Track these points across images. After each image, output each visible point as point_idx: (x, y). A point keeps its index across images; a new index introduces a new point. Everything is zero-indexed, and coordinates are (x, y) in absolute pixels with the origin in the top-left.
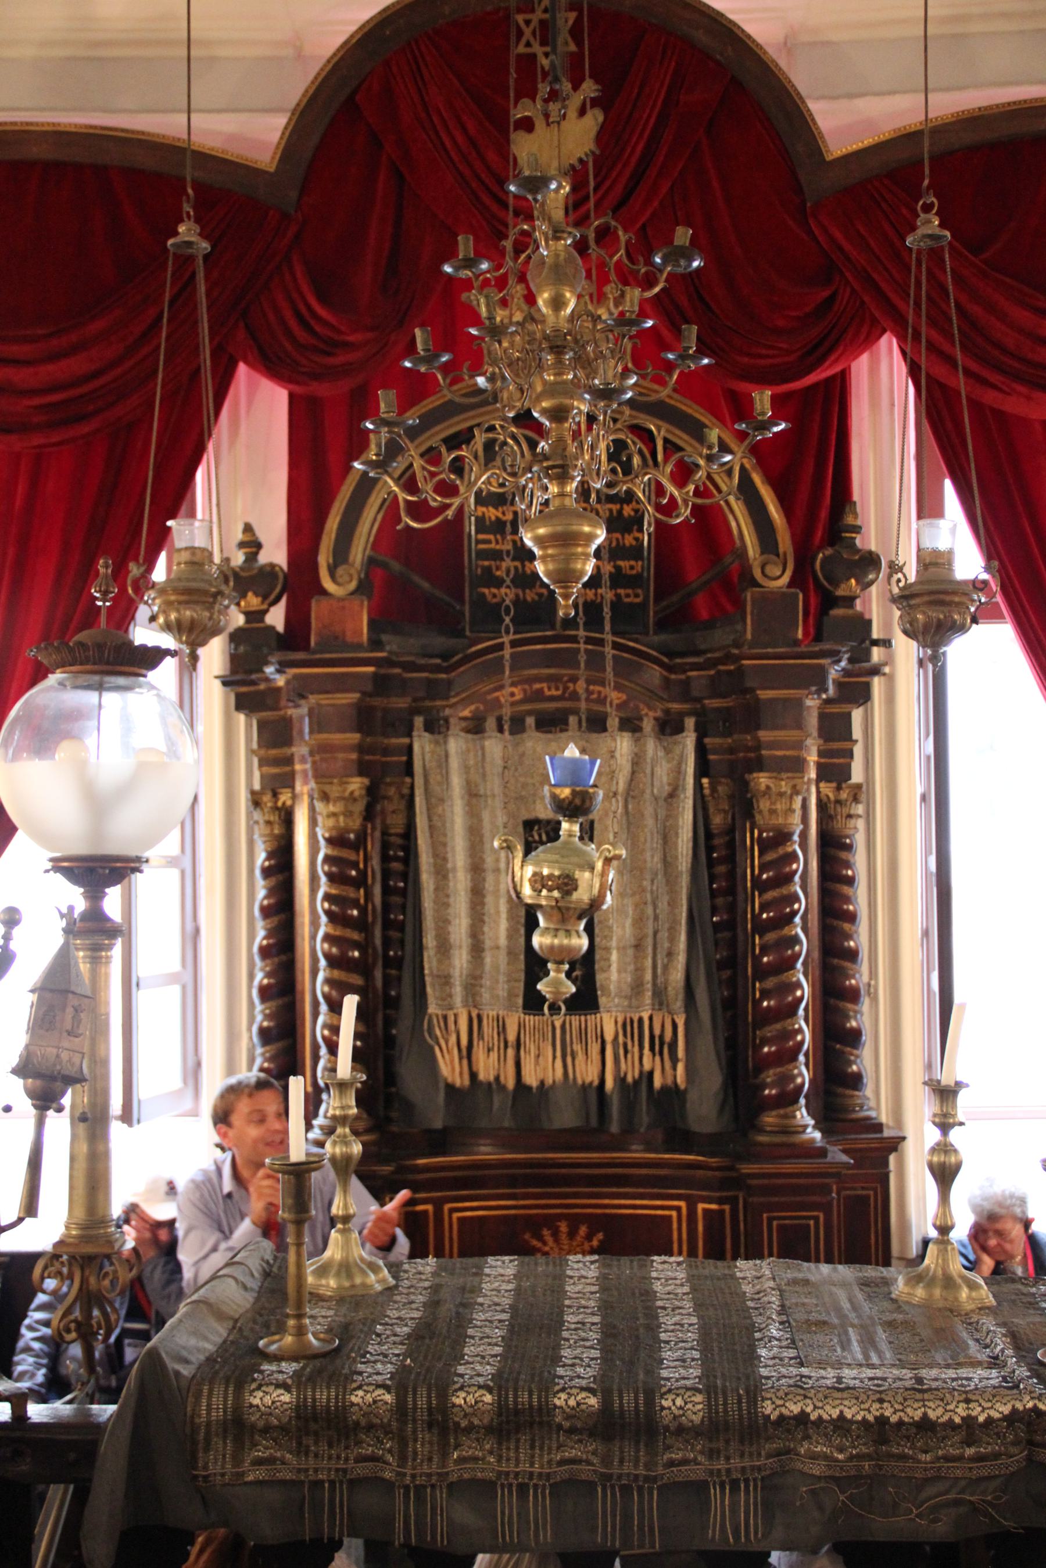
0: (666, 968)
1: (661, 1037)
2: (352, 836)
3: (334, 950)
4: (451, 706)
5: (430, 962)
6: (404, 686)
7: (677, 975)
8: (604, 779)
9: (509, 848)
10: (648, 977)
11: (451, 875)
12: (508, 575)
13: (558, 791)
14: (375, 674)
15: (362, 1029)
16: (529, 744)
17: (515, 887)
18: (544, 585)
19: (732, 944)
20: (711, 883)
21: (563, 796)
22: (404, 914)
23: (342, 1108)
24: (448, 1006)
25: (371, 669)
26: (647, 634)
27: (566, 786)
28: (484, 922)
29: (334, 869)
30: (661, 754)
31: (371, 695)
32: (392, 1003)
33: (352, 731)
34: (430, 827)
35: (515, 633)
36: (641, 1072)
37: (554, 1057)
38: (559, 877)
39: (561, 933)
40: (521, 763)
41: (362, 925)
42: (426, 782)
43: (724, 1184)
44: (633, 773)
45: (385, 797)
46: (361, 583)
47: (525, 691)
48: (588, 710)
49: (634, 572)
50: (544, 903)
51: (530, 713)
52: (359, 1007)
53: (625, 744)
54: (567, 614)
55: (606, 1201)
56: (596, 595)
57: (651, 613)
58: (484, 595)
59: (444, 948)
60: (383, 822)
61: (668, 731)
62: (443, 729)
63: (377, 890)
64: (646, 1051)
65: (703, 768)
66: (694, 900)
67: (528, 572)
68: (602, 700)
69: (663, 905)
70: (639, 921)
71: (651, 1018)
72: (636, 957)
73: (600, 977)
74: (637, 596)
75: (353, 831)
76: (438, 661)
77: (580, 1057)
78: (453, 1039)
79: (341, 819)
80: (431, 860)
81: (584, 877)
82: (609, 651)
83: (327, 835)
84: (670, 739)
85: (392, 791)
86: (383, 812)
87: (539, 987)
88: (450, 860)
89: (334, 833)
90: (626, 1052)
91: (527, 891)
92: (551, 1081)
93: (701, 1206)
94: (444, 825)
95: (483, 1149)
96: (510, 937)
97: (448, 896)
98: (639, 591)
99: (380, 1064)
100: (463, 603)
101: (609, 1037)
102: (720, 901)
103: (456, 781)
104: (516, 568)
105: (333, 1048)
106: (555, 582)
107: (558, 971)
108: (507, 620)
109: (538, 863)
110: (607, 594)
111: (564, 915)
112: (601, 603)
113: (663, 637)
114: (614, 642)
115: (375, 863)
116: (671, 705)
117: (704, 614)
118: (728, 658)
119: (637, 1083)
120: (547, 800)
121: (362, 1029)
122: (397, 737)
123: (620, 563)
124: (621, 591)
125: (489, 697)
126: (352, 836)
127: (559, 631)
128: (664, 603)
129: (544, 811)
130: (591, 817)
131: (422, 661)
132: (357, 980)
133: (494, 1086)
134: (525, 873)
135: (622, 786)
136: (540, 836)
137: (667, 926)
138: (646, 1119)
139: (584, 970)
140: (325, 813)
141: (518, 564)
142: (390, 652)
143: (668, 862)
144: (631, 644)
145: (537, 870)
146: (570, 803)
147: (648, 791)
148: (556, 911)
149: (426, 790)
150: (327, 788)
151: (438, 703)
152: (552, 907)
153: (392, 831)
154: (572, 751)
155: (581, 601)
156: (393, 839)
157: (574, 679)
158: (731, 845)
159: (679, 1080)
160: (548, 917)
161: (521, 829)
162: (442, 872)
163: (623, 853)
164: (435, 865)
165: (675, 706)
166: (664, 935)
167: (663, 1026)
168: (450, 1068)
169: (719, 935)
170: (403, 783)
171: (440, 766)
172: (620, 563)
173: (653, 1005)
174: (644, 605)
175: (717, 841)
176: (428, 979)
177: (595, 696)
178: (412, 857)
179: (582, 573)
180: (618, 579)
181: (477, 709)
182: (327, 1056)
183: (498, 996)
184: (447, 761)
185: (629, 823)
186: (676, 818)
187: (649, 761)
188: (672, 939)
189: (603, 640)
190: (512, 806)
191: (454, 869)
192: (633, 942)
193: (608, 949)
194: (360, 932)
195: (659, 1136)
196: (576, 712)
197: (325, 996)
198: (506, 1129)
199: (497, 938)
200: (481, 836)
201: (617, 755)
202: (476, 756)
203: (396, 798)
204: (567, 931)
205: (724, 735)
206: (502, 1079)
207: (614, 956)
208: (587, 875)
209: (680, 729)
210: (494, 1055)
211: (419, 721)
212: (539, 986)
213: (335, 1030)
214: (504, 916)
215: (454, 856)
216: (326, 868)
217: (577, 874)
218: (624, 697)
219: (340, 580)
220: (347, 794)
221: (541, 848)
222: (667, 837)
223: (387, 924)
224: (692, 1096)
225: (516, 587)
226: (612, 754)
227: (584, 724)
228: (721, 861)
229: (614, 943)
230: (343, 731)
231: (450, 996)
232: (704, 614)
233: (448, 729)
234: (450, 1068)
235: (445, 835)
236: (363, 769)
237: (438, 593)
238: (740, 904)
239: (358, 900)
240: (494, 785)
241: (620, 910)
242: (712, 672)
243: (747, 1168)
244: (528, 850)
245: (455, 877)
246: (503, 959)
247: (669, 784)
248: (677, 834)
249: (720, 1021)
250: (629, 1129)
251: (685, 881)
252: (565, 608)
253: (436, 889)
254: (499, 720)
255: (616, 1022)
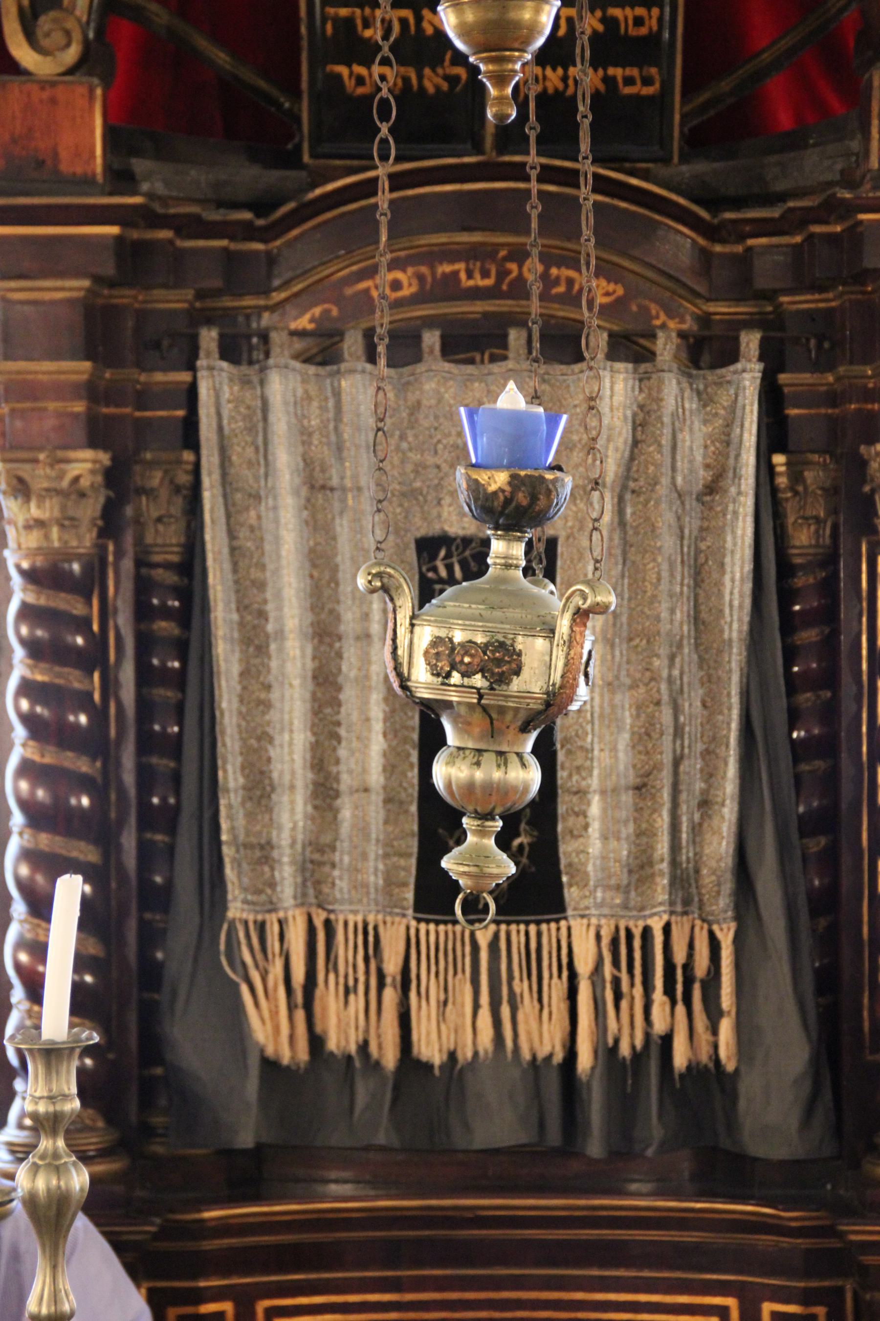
0: (696, 830)
1: (688, 967)
2: (76, 567)
3: (40, 793)
4: (272, 309)
5: (230, 817)
6: (177, 268)
7: (720, 845)
8: (577, 456)
9: (385, 589)
10: (663, 847)
11: (273, 647)
12: (385, 37)
13: (483, 477)
14: (119, 240)
15: (94, 948)
16: (429, 386)
17: (399, 675)
18: (460, 58)
19: (830, 783)
20: (788, 663)
21: (493, 488)
22: (181, 724)
23: (51, 1098)
24: (266, 901)
25: (114, 230)
26: (666, 160)
27: (498, 467)
28: (339, 739)
29: (39, 633)
30: (692, 404)
31: (112, 284)
32: (156, 899)
33: (73, 357)
34: (233, 550)
35: (399, 159)
36: (647, 1036)
37: (476, 1006)
38: (485, 647)
39: (489, 759)
40: (413, 424)
41: (96, 743)
42: (223, 451)
43: (816, 1263)
44: (636, 443)
45: (142, 491)
46: (87, 44)
47: (421, 278)
48: (546, 318)
49: (643, 31)
50: (454, 697)
51: (430, 322)
52: (86, 903)
53: (619, 387)
54: (501, 117)
55: (579, 1296)
56: (565, 79)
57: (677, 117)
58: (339, 77)
59: (260, 790)
60: (139, 541)
61: (706, 358)
62: (257, 355)
63: (127, 674)
64: (658, 995)
65: (775, 434)
66: (754, 696)
67: (429, 31)
68: (572, 298)
69: (692, 704)
70: (644, 738)
71: (667, 930)
72: (638, 810)
73: (566, 849)
74: (647, 81)
75: (78, 557)
76: (247, 215)
77: (528, 1007)
78: (276, 970)
79: (55, 532)
80: (235, 617)
81: (533, 649)
82: (587, 196)
83: (25, 565)
84: (711, 376)
85: (156, 479)
86: (138, 522)
87: (445, 863)
88: (272, 615)
89: (39, 562)
90: (618, 996)
91: (421, 675)
92: (469, 1055)
93: (767, 1308)
94: (260, 547)
95: (333, 1188)
96: (389, 769)
97: (268, 687)
98: (654, 71)
99: (132, 1018)
100: (295, 93)
101: (584, 966)
102: (806, 698)
103: (284, 459)
104: (403, 22)
105: (35, 990)
106: (480, 49)
107: (482, 832)
108: (384, 129)
109: (443, 621)
110: (586, 78)
111: (493, 721)
112: (574, 97)
113: (701, 167)
114: (596, 176)
115: (123, 619)
116: (712, 308)
117: (785, 120)
118: (832, 209)
119: (638, 1057)
120: (463, 497)
121: (94, 948)
122: (165, 370)
123: (616, 12)
124: (617, 72)
125: (349, 291)
126: (76, 567)
127: (490, 154)
128: (704, 96)
129: (458, 520)
130: (550, 530)
131: (214, 216)
132: (89, 854)
133: (357, 1064)
134: (418, 640)
135: (612, 469)
136: (450, 568)
137: (700, 747)
138: (657, 1132)
139: (535, 826)
140: (21, 521)
141: (407, 13)
142: (150, 196)
143: (702, 622)
144: (634, 181)
145: (443, 633)
146: (508, 501)
147: (665, 481)
148: (478, 717)
149: (224, 475)
150: (25, 471)
151: (249, 301)
152: (470, 706)
153: (157, 558)
154: (511, 398)
155: (534, 91)
156: (159, 574)
157: (519, 255)
158: (829, 588)
159: (723, 1053)
160: (463, 727)
161: (411, 554)
162: (256, 641)
163: (612, 599)
164: (242, 624)
165: (720, 309)
166: (692, 766)
167: (691, 946)
168: (270, 1028)
169: (804, 767)
170: (179, 462)
171: (251, 430)
172: (616, 12)
173: (672, 903)
174: (662, 101)
175: (801, 581)
176: (227, 852)
177: (561, 289)
178: (196, 610)
179: (533, 29)
180: (609, 47)
181: (327, 312)
182: (26, 1005)
183: (365, 885)
184: (265, 419)
185: (626, 545)
186: (720, 533)
187: (666, 420)
188: (710, 775)
189: (576, 172)
190: (394, 509)
191: (280, 634)
192: (632, 779)
193: (581, 793)
194: (94, 759)
195: (684, 1164)
196: (520, 320)
197: (21, 885)
198: (382, 1149)
199: (365, 771)
200: (335, 569)
201: (604, 406)
202: (323, 409)
203: (164, 493)
204: (500, 754)
205: (820, 366)
206: (373, 1048)
207: (595, 808)
208: (540, 643)
209: (729, 355)
210: (357, 1002)
211: (209, 337)
212: (446, 863)
213: (39, 950)
214: (378, 726)
215: (280, 609)
216: (24, 631)
217: (521, 643)
218: (620, 291)
219: (45, 43)
220: (65, 483)
221: (450, 591)
222: (701, 571)
223: (147, 743)
224: (749, 1088)
225: (401, 62)
226: (592, 403)
227: (537, 345)
228: (808, 619)
229: (594, 782)
230: (57, 356)
231: (272, 885)
232: (785, 120)
233: (267, 355)
234: (270, 1028)
235: (263, 567)
236: (97, 434)
237: (247, 75)
238: (847, 706)
239: (90, 695)
240: (358, 468)
241: (611, 718)
242: (798, 239)
243: (860, 1232)
244: (426, 592)
245: (281, 650)
246: (375, 813)
247: (707, 466)
248: (722, 565)
249: (806, 941)
250: (624, 1148)
251: (735, 660)
252: (498, 106)
253: (245, 674)
254: (369, 334)
255: (598, 937)
